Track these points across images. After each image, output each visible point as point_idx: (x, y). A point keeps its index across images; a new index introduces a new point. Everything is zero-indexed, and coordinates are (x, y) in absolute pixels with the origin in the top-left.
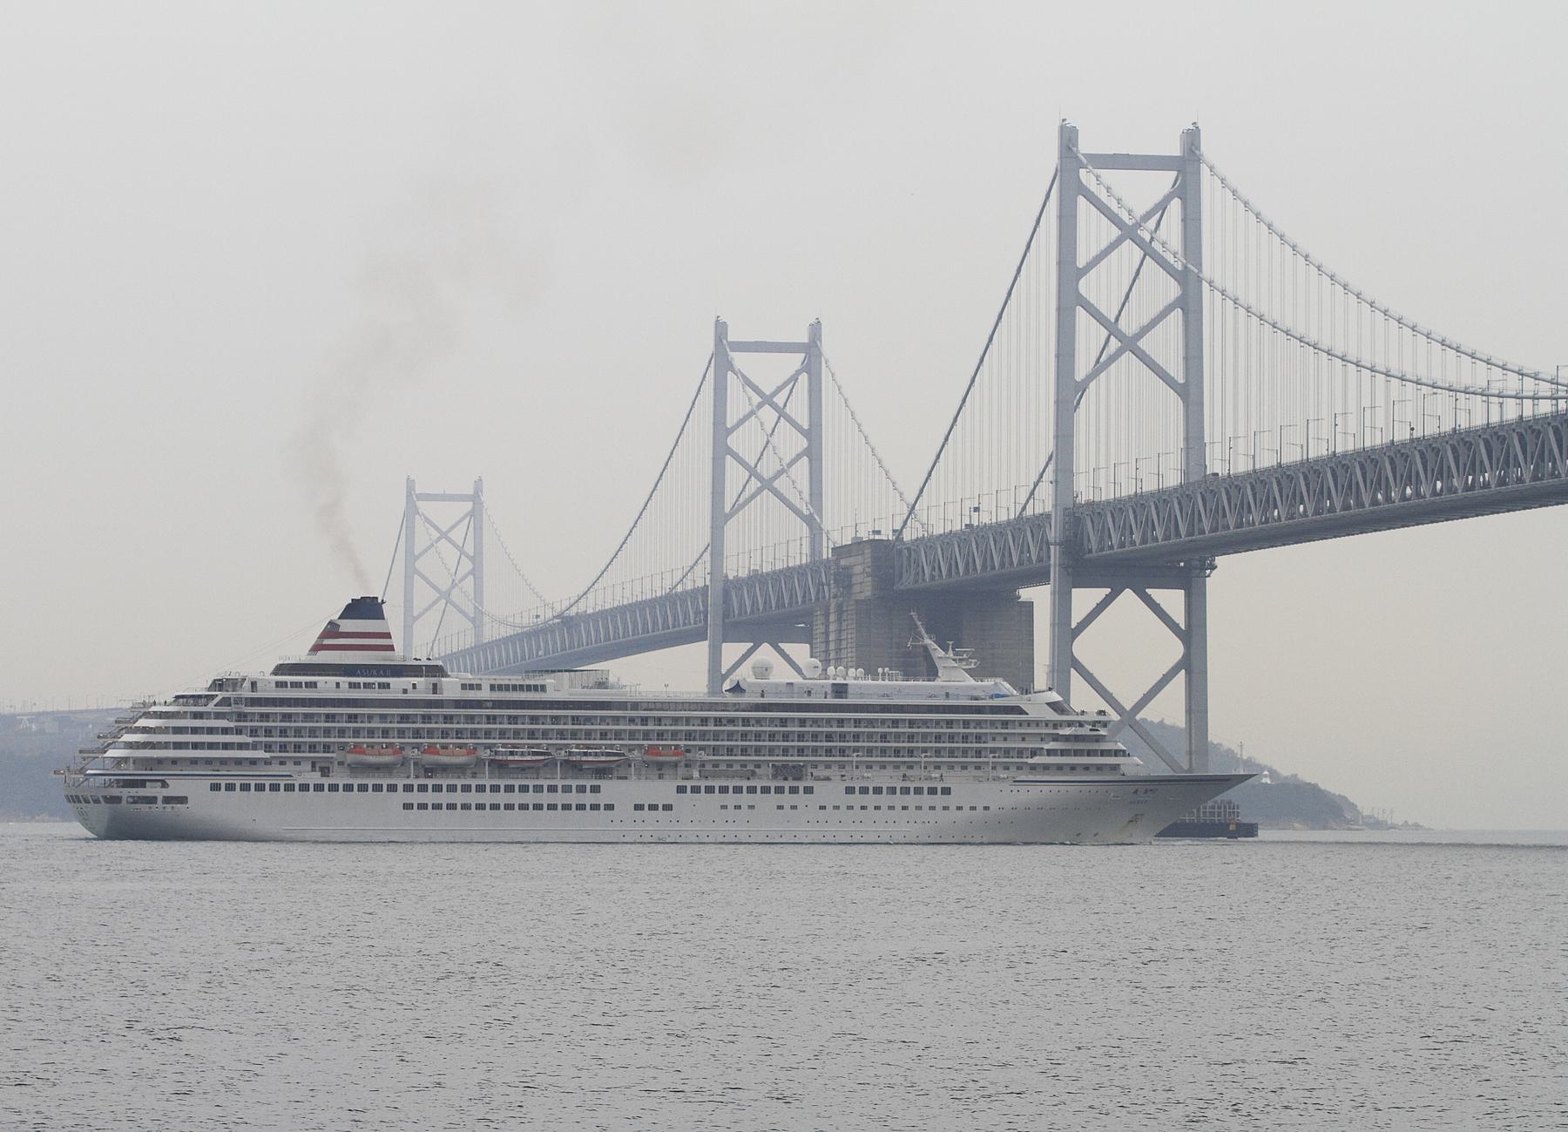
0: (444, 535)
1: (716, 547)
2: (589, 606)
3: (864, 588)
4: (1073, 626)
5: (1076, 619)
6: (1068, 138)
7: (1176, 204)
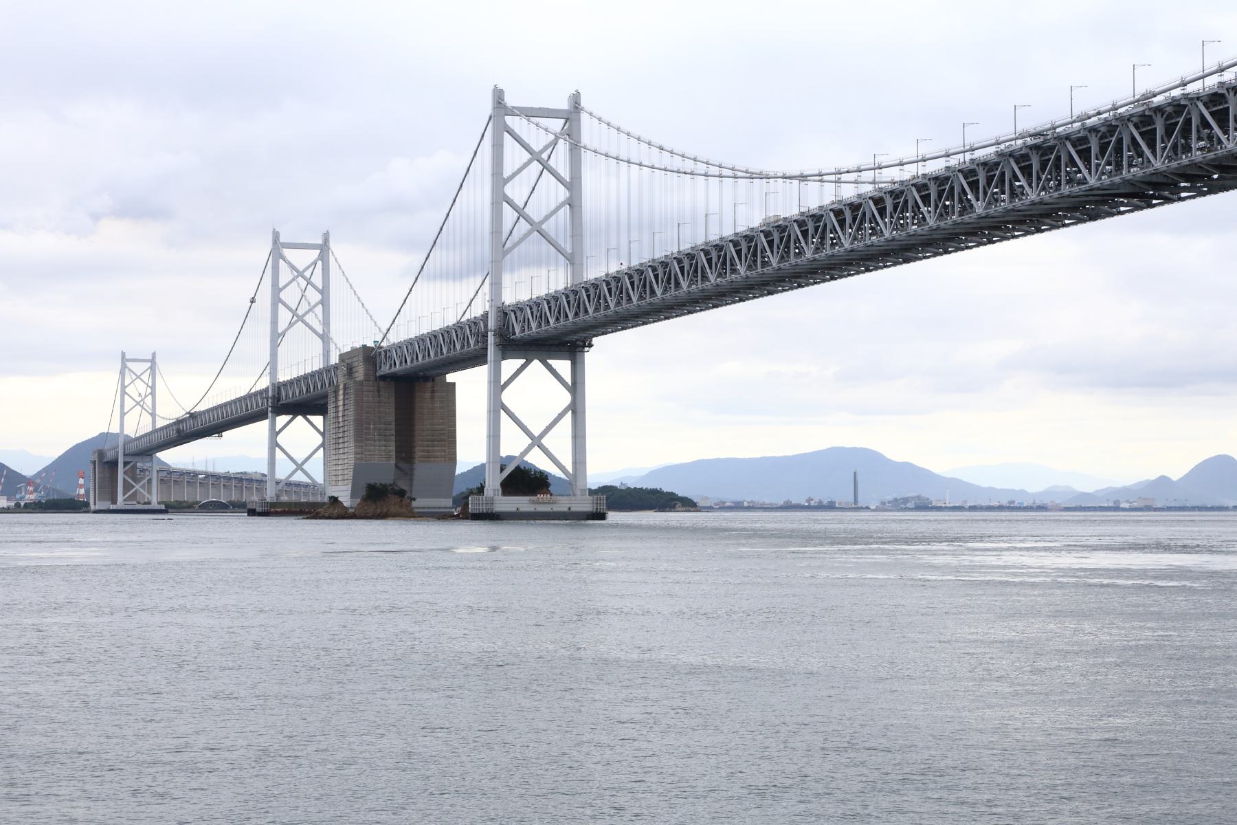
0: (138, 377)
1: (273, 364)
2: (202, 407)
3: (360, 374)
4: (502, 384)
5: (504, 379)
6: (499, 96)
7: (320, 263)
